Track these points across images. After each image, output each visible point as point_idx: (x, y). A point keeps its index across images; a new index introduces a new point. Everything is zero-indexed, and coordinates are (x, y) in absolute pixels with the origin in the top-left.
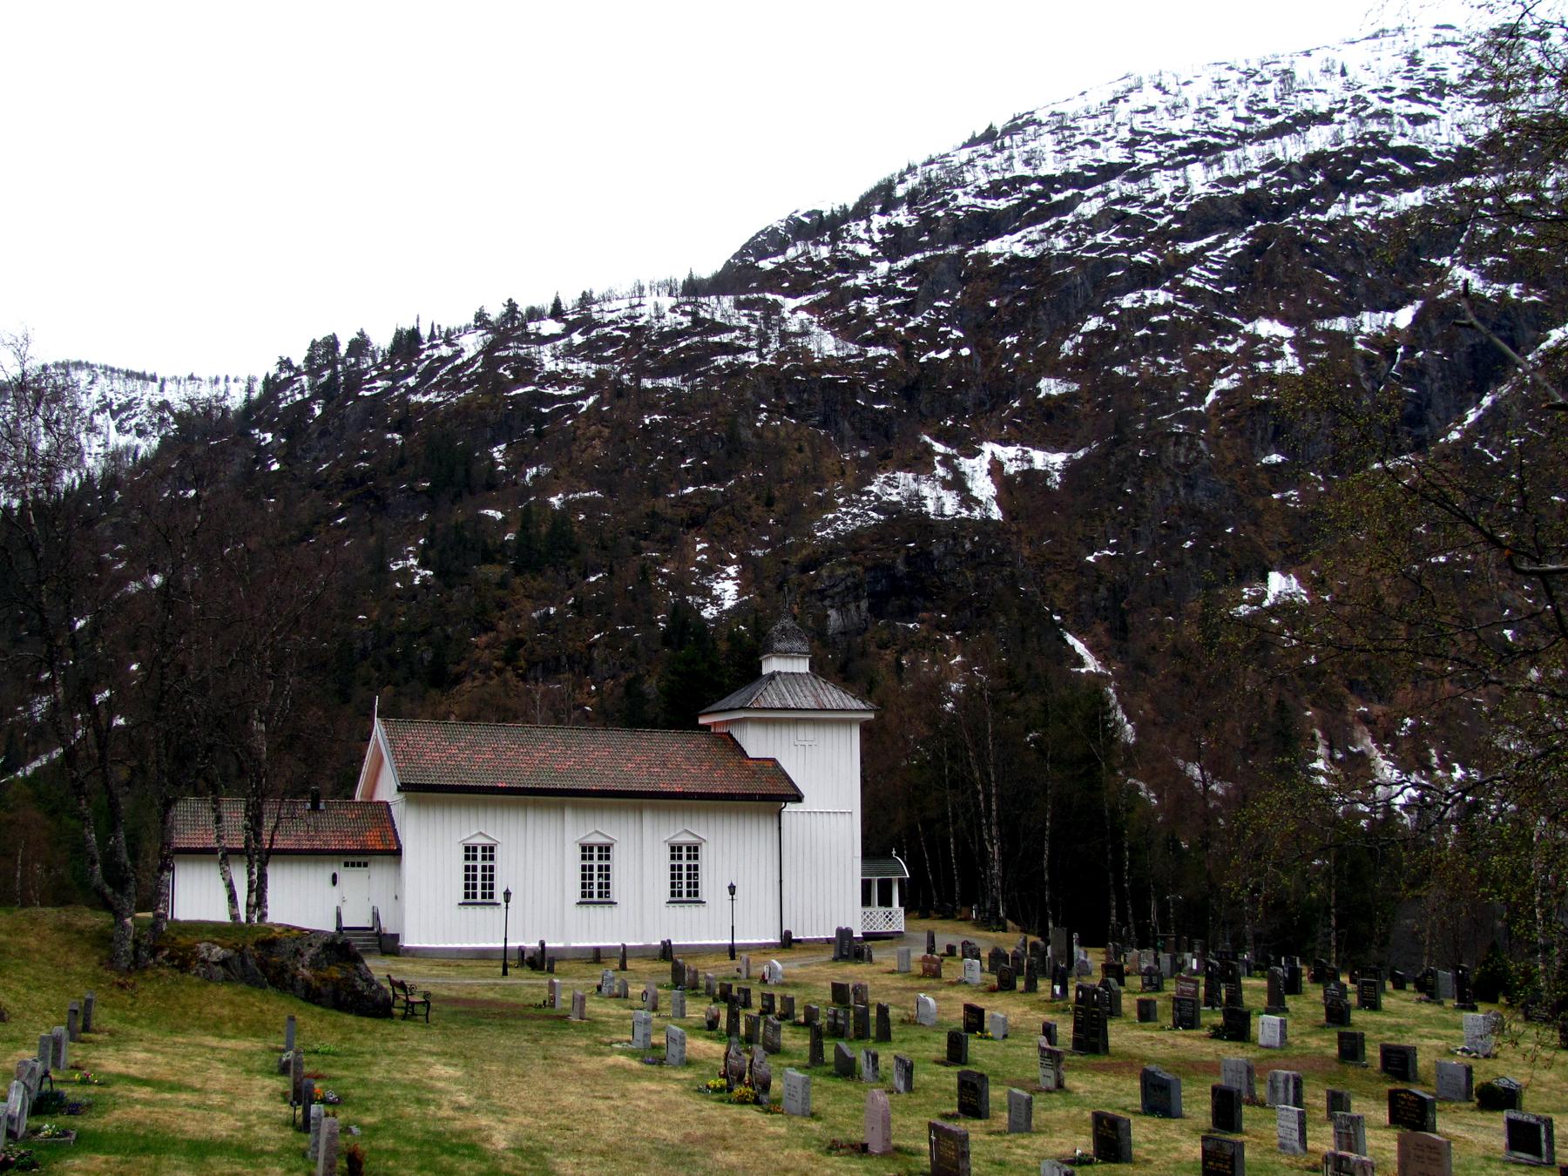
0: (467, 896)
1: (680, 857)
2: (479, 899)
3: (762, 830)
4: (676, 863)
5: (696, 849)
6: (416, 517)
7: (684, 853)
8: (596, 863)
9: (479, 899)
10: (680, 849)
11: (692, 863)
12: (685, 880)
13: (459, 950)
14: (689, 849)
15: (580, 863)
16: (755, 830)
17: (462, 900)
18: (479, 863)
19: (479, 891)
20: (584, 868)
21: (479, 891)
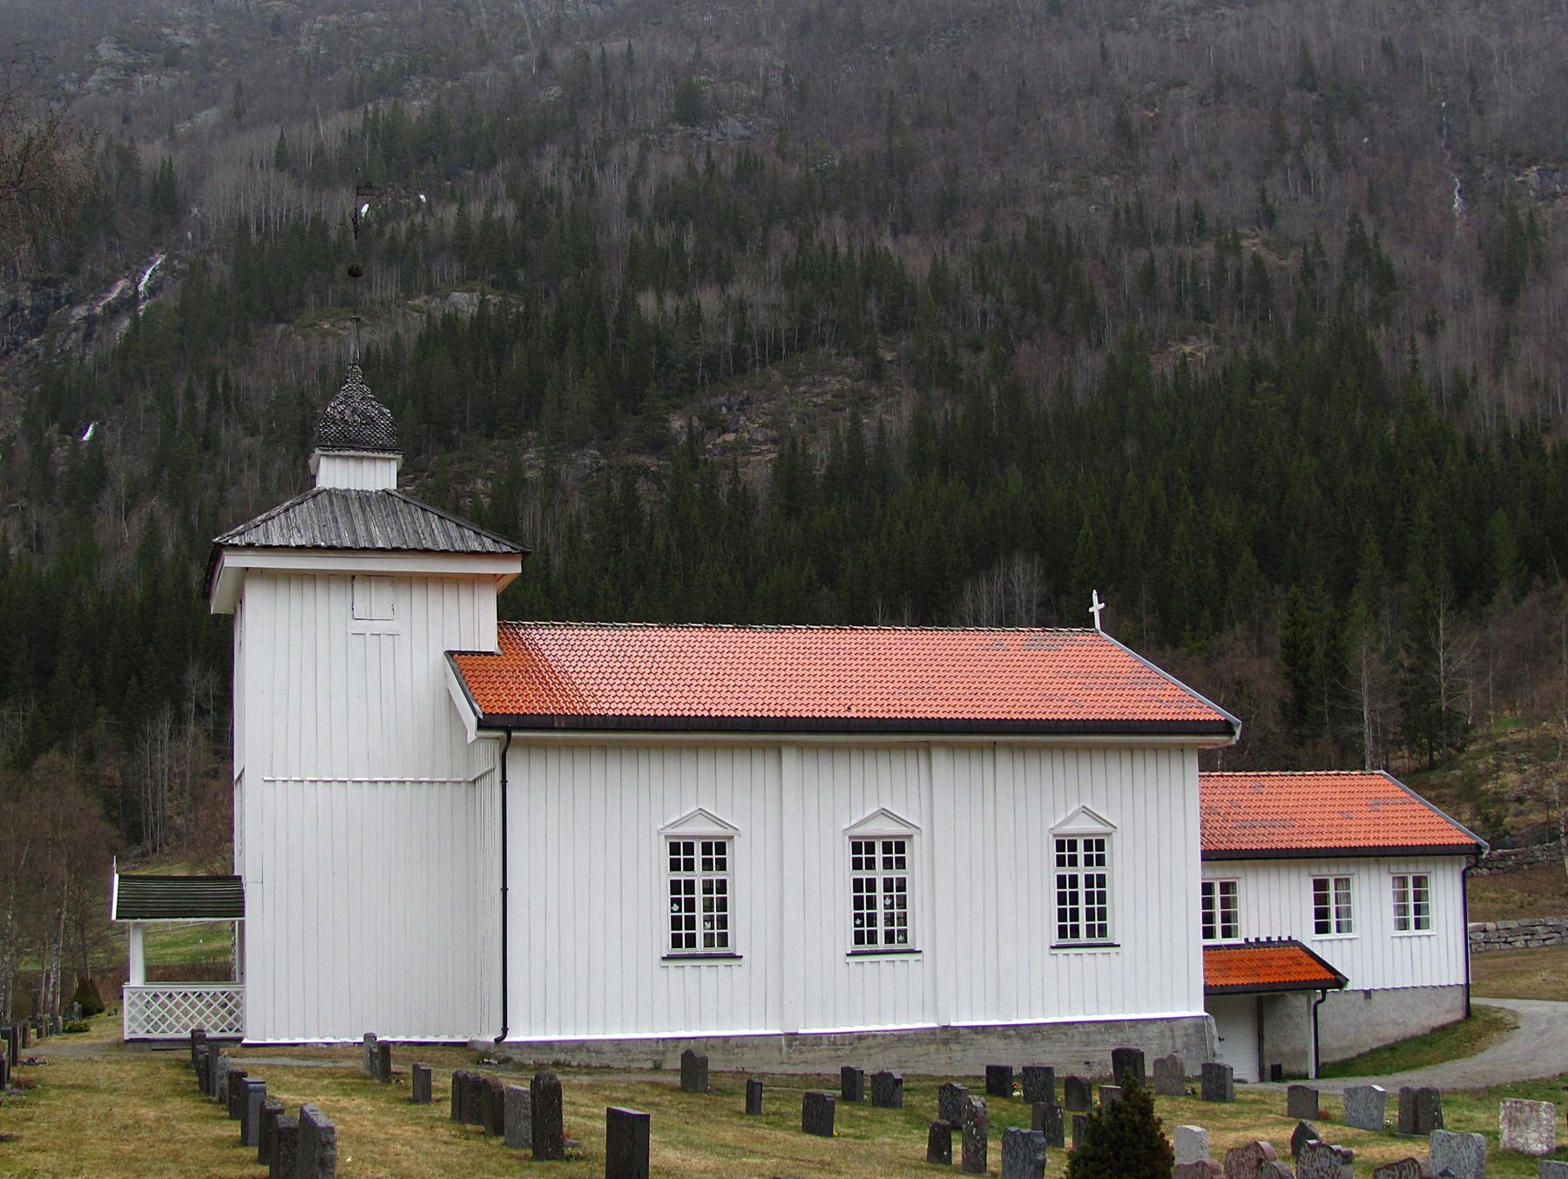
0: (676, 941)
1: (689, 866)
2: (881, 943)
3: (1059, 777)
4: (682, 876)
5: (901, 847)
6: (77, 443)
7: (698, 856)
8: (1081, 871)
9: (700, 947)
10: (870, 848)
11: (895, 874)
12: (880, 912)
13: (917, 1031)
14: (887, 848)
15: (667, 876)
16: (1059, 777)
17: (1056, 940)
18: (699, 876)
19: (1082, 923)
20: (857, 885)
21: (1082, 923)
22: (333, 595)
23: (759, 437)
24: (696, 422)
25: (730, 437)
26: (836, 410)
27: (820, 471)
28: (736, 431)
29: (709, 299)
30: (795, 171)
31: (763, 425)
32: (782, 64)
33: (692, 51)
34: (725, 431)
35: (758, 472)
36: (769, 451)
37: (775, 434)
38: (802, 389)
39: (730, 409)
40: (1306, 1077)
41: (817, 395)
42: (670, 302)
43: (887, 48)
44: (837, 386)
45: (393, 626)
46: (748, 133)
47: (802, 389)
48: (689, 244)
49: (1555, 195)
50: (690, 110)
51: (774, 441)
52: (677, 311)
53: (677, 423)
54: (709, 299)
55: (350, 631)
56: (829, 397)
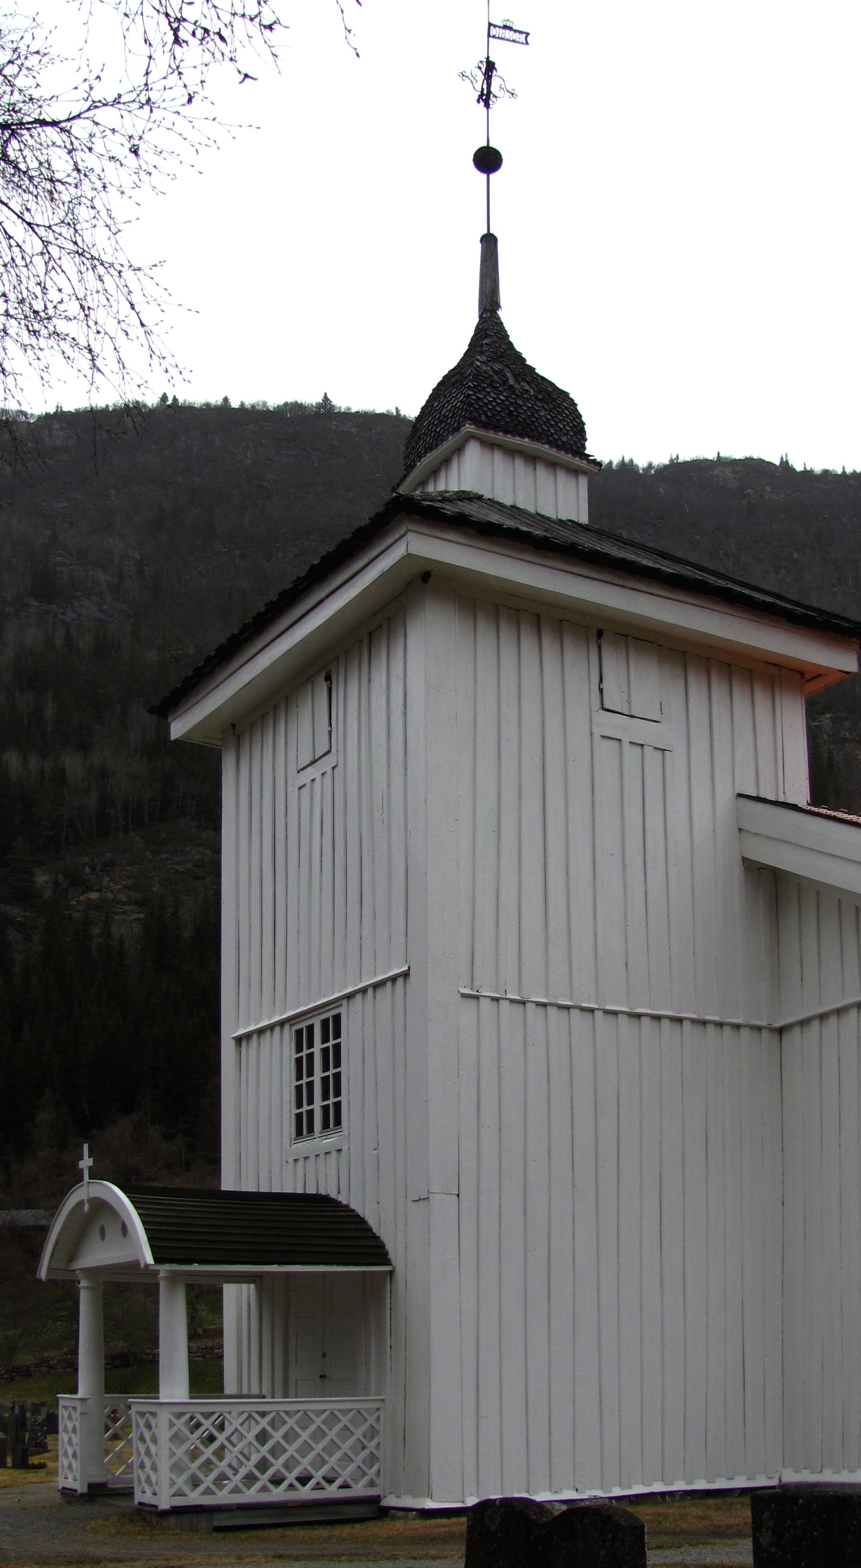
22: (567, 642)
23: (122, 897)
24: (61, 878)
25: (94, 895)
26: (197, 878)
27: (187, 934)
28: (97, 891)
29: (73, 764)
30: (152, 656)
31: (126, 887)
32: (137, 555)
33: (48, 533)
34: (89, 889)
35: (128, 925)
36: (133, 912)
37: (138, 896)
38: (164, 856)
39: (93, 869)
40: (242, 1424)
41: (179, 863)
42: (34, 763)
43: (238, 552)
44: (198, 857)
45: (664, 734)
46: (102, 616)
47: (164, 856)
48: (50, 711)
49: (845, 740)
50: (47, 588)
51: (138, 903)
52: (42, 771)
53: (42, 878)
54: (73, 764)
55: (598, 731)
56: (190, 865)
